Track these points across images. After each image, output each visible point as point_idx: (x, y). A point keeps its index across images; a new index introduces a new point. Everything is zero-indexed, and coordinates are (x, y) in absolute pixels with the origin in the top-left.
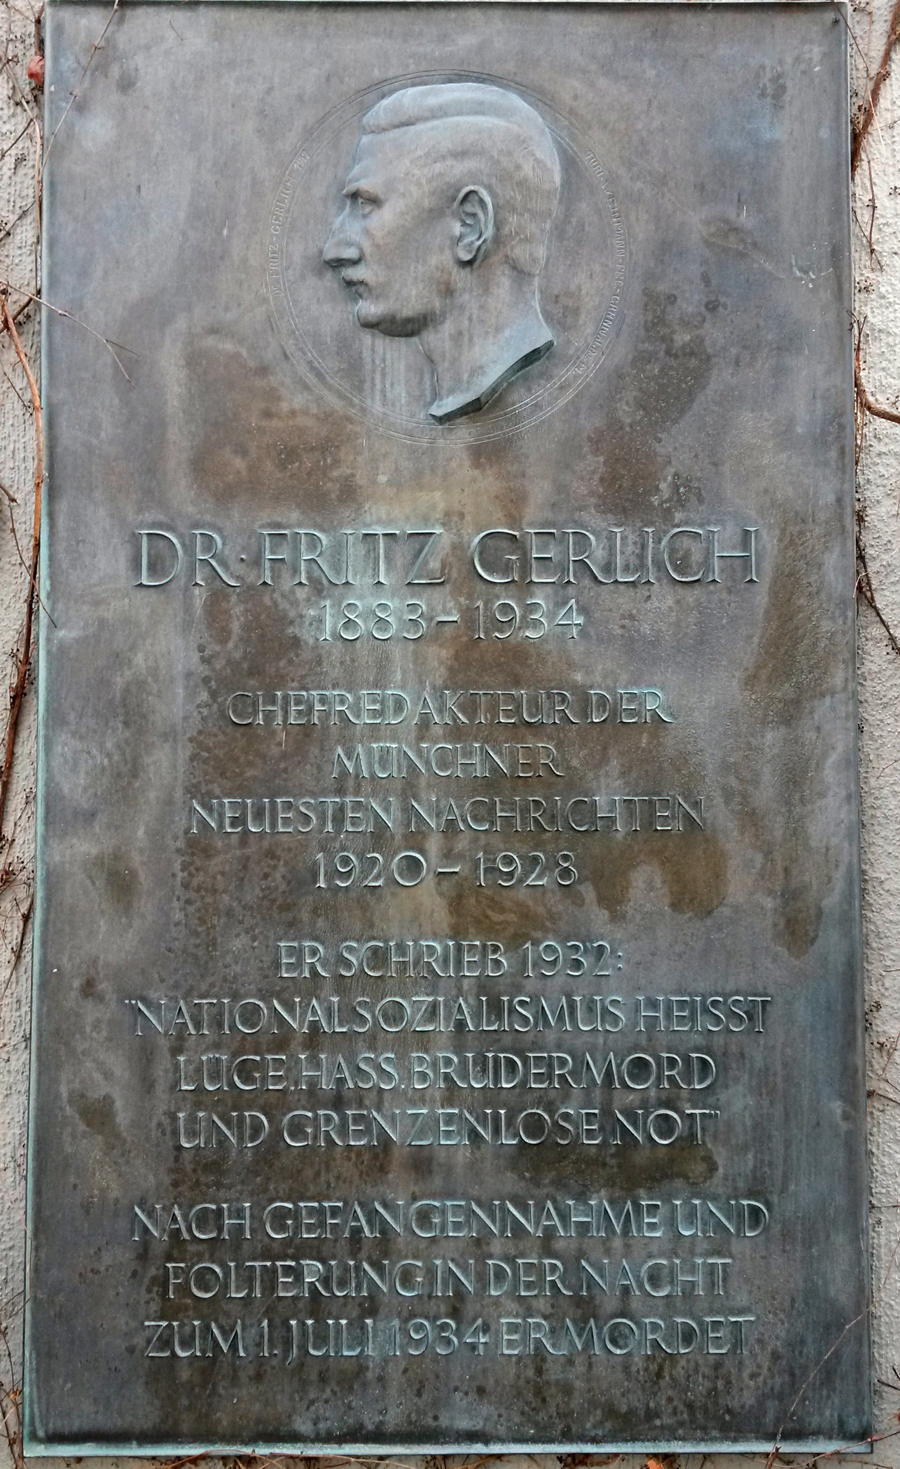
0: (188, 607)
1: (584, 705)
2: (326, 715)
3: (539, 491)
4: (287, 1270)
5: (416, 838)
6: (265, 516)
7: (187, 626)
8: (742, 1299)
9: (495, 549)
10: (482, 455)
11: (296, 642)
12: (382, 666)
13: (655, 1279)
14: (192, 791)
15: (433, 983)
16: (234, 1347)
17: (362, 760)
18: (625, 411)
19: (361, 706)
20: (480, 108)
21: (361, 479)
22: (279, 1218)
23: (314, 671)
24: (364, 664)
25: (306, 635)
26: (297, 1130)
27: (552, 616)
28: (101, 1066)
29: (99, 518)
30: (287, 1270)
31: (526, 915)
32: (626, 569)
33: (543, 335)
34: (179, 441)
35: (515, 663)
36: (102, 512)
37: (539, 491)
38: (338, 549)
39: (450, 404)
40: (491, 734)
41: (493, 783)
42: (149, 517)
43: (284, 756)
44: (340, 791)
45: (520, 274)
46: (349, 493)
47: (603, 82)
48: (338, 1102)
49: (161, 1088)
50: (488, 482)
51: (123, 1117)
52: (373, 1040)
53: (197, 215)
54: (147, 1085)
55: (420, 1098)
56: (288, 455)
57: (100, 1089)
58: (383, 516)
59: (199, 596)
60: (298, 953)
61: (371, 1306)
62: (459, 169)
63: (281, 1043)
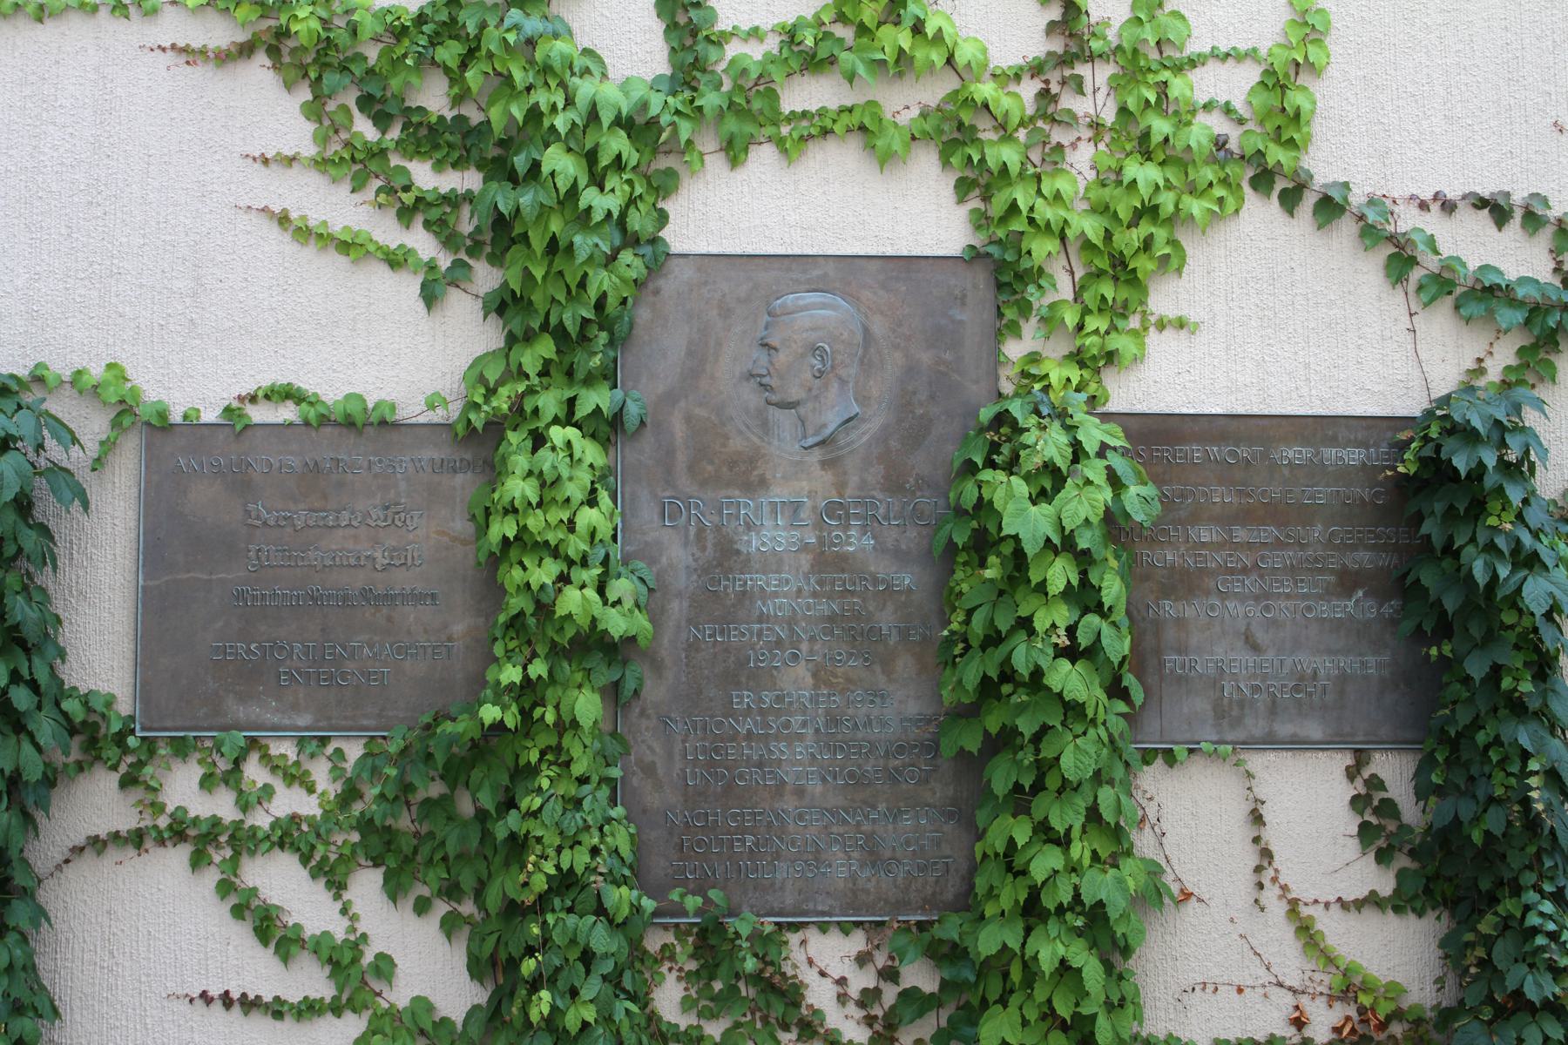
0: (687, 537)
1: (876, 581)
2: (752, 587)
3: (854, 480)
4: (738, 840)
5: (795, 644)
6: (724, 492)
7: (686, 544)
8: (948, 852)
9: (831, 509)
10: (825, 464)
11: (738, 552)
12: (780, 562)
13: (908, 843)
14: (689, 621)
15: (804, 712)
16: (714, 874)
17: (769, 608)
18: (894, 444)
19: (771, 583)
20: (824, 306)
21: (768, 476)
22: (734, 816)
23: (746, 566)
24: (771, 563)
25: (744, 550)
26: (741, 777)
27: (859, 540)
28: (650, 747)
29: (644, 495)
30: (738, 840)
31: (849, 680)
32: (895, 518)
33: (856, 409)
34: (681, 458)
35: (843, 562)
36: (1310, 800)
37: (854, 480)
38: (759, 507)
39: (811, 441)
40: (830, 596)
41: (832, 618)
42: (667, 494)
43: (733, 606)
44: (760, 622)
45: (843, 382)
46: (763, 483)
47: (881, 292)
48: (760, 765)
49: (677, 758)
50: (829, 476)
51: (660, 771)
52: (777, 737)
53: (690, 353)
54: (670, 756)
55: (800, 763)
56: (732, 464)
57: (649, 758)
58: (780, 493)
59: (692, 531)
60: (741, 697)
61: (777, 856)
62: (813, 336)
63: (733, 738)
